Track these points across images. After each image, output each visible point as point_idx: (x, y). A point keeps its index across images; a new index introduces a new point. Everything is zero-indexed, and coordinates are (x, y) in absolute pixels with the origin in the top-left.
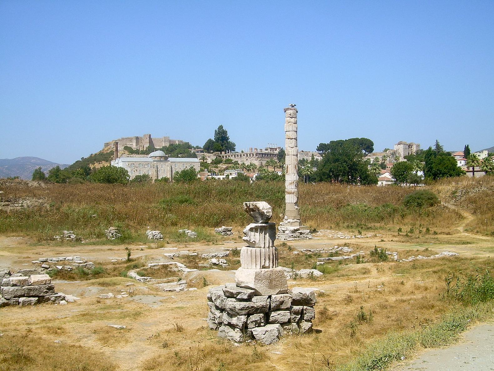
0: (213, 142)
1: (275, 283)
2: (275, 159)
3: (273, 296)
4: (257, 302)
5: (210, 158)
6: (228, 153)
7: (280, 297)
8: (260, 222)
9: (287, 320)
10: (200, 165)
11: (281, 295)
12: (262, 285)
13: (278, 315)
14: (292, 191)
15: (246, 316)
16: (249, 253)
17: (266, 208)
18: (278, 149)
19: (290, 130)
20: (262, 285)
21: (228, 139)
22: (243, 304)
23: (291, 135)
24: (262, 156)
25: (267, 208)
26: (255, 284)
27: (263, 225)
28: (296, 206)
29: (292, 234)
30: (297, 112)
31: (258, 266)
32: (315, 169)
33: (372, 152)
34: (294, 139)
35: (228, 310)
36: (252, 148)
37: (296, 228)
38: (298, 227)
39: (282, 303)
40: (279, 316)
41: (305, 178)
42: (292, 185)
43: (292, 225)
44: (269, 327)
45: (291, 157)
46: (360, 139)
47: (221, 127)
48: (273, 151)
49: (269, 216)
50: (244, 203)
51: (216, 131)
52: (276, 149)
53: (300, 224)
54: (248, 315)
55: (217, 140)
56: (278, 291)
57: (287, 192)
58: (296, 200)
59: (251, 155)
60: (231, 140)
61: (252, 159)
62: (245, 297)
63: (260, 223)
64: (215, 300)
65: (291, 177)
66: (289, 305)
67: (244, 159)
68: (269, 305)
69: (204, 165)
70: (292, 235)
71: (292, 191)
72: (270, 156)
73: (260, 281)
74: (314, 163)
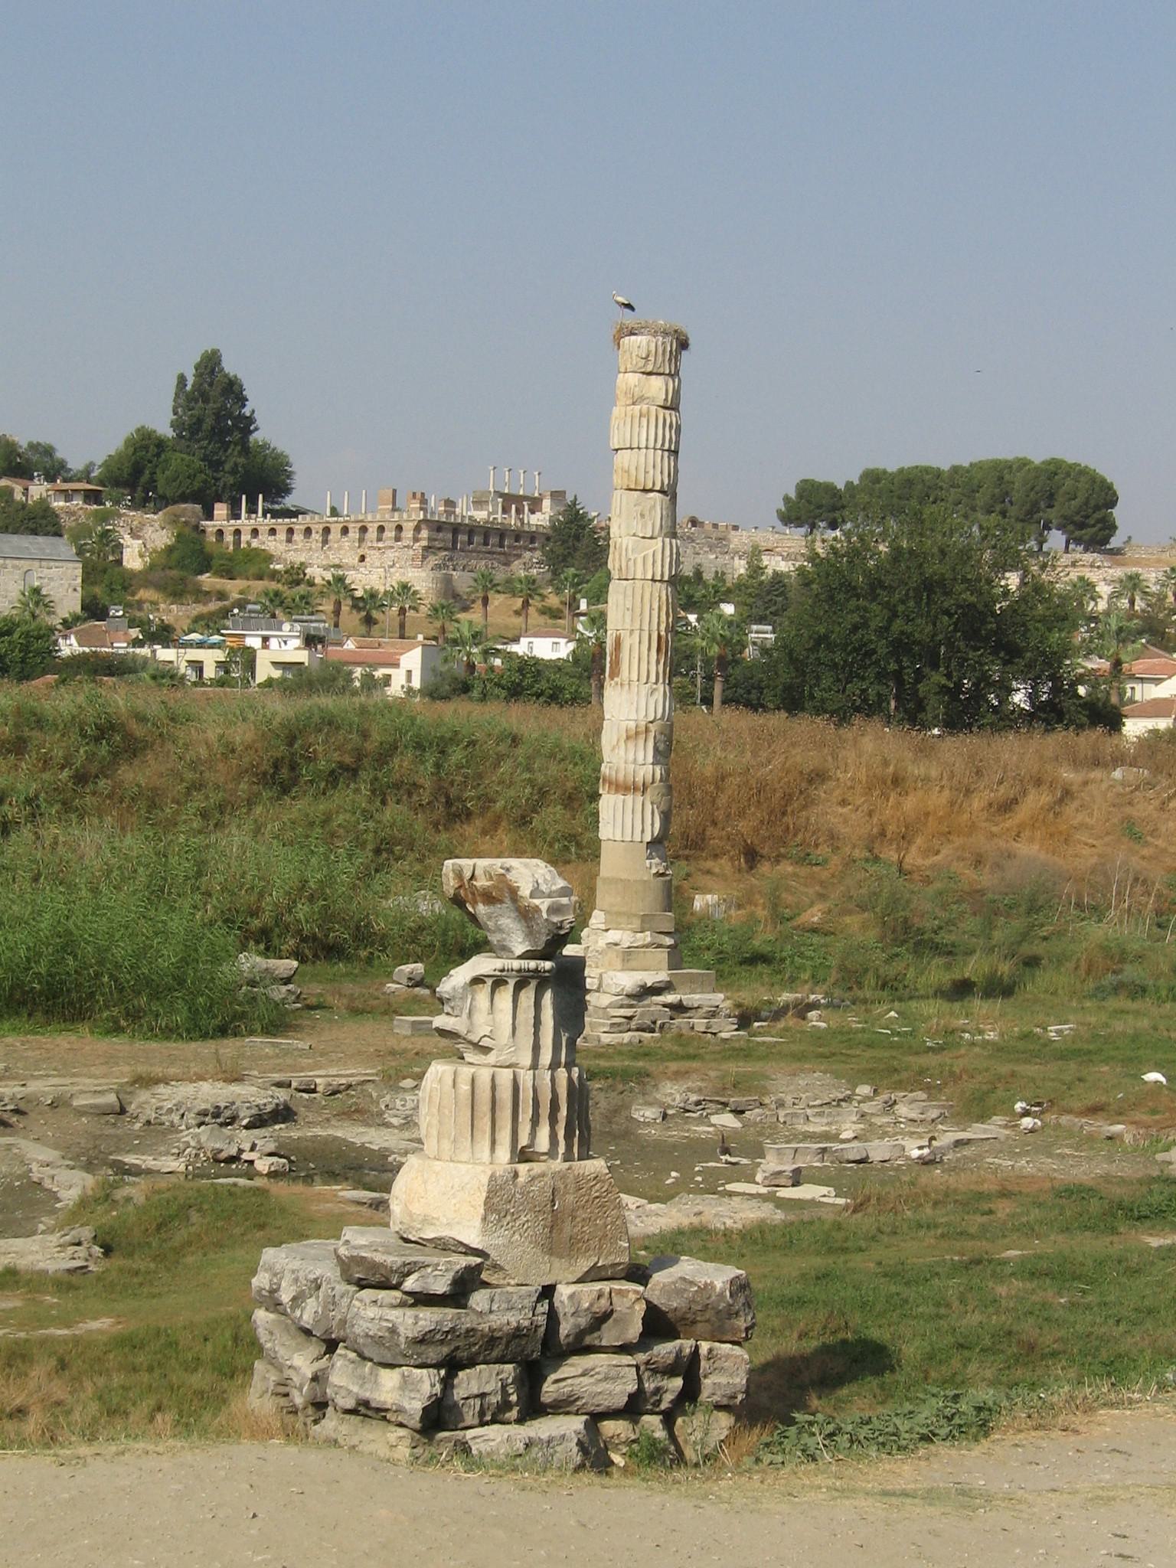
0: (161, 444)
1: (576, 1230)
2: (529, 565)
3: (564, 1292)
4: (497, 1310)
5: (142, 540)
6: (252, 510)
7: (595, 1295)
8: (518, 952)
9: (621, 1401)
10: (79, 580)
11: (598, 1286)
12: (517, 1236)
13: (583, 1375)
14: (639, 780)
15: (443, 1372)
16: (465, 1088)
17: (547, 891)
18: (547, 503)
19: (635, 445)
20: (517, 1236)
21: (246, 425)
22: (428, 1318)
23: (646, 472)
24: (455, 542)
25: (554, 888)
26: (484, 1232)
27: (533, 964)
28: (657, 860)
29: (628, 1012)
30: (683, 345)
31: (504, 1153)
32: (762, 634)
33: (1108, 542)
34: (661, 492)
35: (361, 1341)
36: (395, 491)
37: (651, 978)
38: (663, 976)
39: (600, 1320)
40: (585, 1380)
41: (699, 673)
42: (641, 742)
43: (633, 964)
44: (543, 1428)
45: (638, 592)
46: (1037, 468)
47: (210, 364)
48: (519, 511)
49: (561, 928)
50: (449, 863)
51: (182, 380)
52: (535, 505)
53: (675, 963)
54: (452, 1366)
55: (189, 428)
56: (584, 1265)
57: (610, 783)
58: (657, 825)
59: (390, 534)
60: (269, 432)
61: (391, 554)
62: (441, 1286)
63: (520, 957)
64: (294, 1299)
65: (632, 704)
66: (634, 1330)
67: (344, 551)
68: (543, 1329)
69: (105, 587)
70: (630, 1018)
71: (639, 780)
72: (501, 545)
73: (509, 1218)
74: (765, 596)
